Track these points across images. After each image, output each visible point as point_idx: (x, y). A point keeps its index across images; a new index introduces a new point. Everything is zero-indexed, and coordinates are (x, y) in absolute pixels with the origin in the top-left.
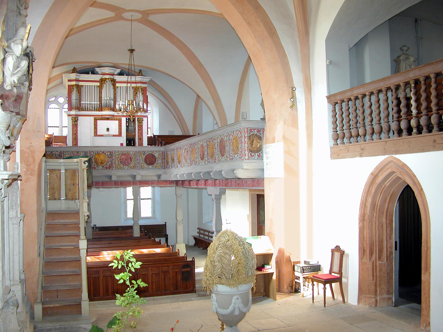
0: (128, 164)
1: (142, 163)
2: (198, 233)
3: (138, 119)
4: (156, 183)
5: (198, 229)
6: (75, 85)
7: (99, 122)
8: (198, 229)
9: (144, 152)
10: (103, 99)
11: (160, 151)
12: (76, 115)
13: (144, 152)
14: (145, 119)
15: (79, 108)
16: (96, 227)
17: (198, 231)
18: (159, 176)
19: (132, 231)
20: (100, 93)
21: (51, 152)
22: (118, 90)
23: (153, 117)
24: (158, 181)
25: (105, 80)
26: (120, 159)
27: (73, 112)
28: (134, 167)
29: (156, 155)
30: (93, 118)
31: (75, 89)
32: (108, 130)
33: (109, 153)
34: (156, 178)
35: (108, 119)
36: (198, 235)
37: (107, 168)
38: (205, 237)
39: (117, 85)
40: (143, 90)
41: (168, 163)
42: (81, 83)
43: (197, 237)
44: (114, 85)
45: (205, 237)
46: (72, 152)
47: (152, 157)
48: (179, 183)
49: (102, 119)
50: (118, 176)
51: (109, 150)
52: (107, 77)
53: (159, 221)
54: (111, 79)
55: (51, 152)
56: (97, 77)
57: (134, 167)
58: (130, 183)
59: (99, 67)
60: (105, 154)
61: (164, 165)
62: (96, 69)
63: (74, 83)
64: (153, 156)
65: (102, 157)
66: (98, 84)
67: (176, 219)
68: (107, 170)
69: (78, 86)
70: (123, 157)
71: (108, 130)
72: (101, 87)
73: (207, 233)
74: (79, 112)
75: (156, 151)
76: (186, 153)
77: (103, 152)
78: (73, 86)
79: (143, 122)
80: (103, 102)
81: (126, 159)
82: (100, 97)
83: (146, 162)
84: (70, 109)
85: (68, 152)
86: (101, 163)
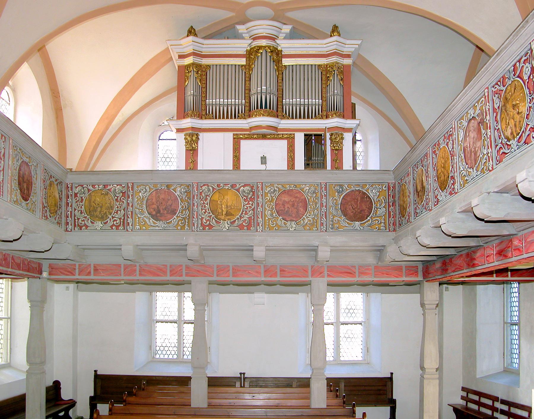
0: (297, 217)
1: (334, 216)
2: (462, 398)
3: (331, 135)
4: (373, 271)
5: (463, 389)
6: (193, 64)
7: (243, 143)
8: (463, 389)
9: (341, 186)
10: (252, 92)
11: (381, 184)
12: (193, 128)
13: (341, 186)
14: (348, 137)
15: (202, 111)
16: (245, 378)
17: (464, 394)
18: (380, 251)
19: (309, 393)
20: (248, 79)
21: (105, 186)
22: (286, 73)
23: (366, 151)
24: (376, 267)
25: (257, 52)
26: (276, 205)
27: (188, 123)
28: (312, 226)
29: (371, 195)
30: (230, 135)
31: (192, 75)
32: (264, 160)
33: (247, 188)
34: (370, 260)
35: (264, 137)
36: (463, 403)
37: (241, 227)
38: (483, 410)
39: (286, 62)
40: (342, 72)
41: (403, 211)
42: (205, 61)
43: (459, 408)
44: (278, 62)
45: (483, 410)
46: (155, 185)
47: (362, 198)
48: (431, 270)
49: (250, 137)
50: (268, 250)
51: (248, 181)
52: (263, 43)
53: (377, 370)
54: (269, 47)
55: (105, 186)
56: (241, 46)
57: (312, 225)
58: (306, 271)
59: (243, 23)
60: (238, 190)
61: (392, 220)
62: (238, 27)
63: (189, 61)
64: (364, 196)
65: (229, 199)
66: (243, 61)
67: (422, 368)
68: (240, 233)
69: (198, 67)
70: (286, 198)
71: (264, 160)
72: (248, 68)
73: (489, 402)
74: (201, 121)
75: (372, 185)
76: (473, 134)
77: (233, 186)
78: (188, 66)
79: (344, 142)
80: (254, 99)
81: (293, 205)
82: (248, 91)
83: (345, 213)
84: (182, 113)
85: (145, 185)
86: (228, 214)
